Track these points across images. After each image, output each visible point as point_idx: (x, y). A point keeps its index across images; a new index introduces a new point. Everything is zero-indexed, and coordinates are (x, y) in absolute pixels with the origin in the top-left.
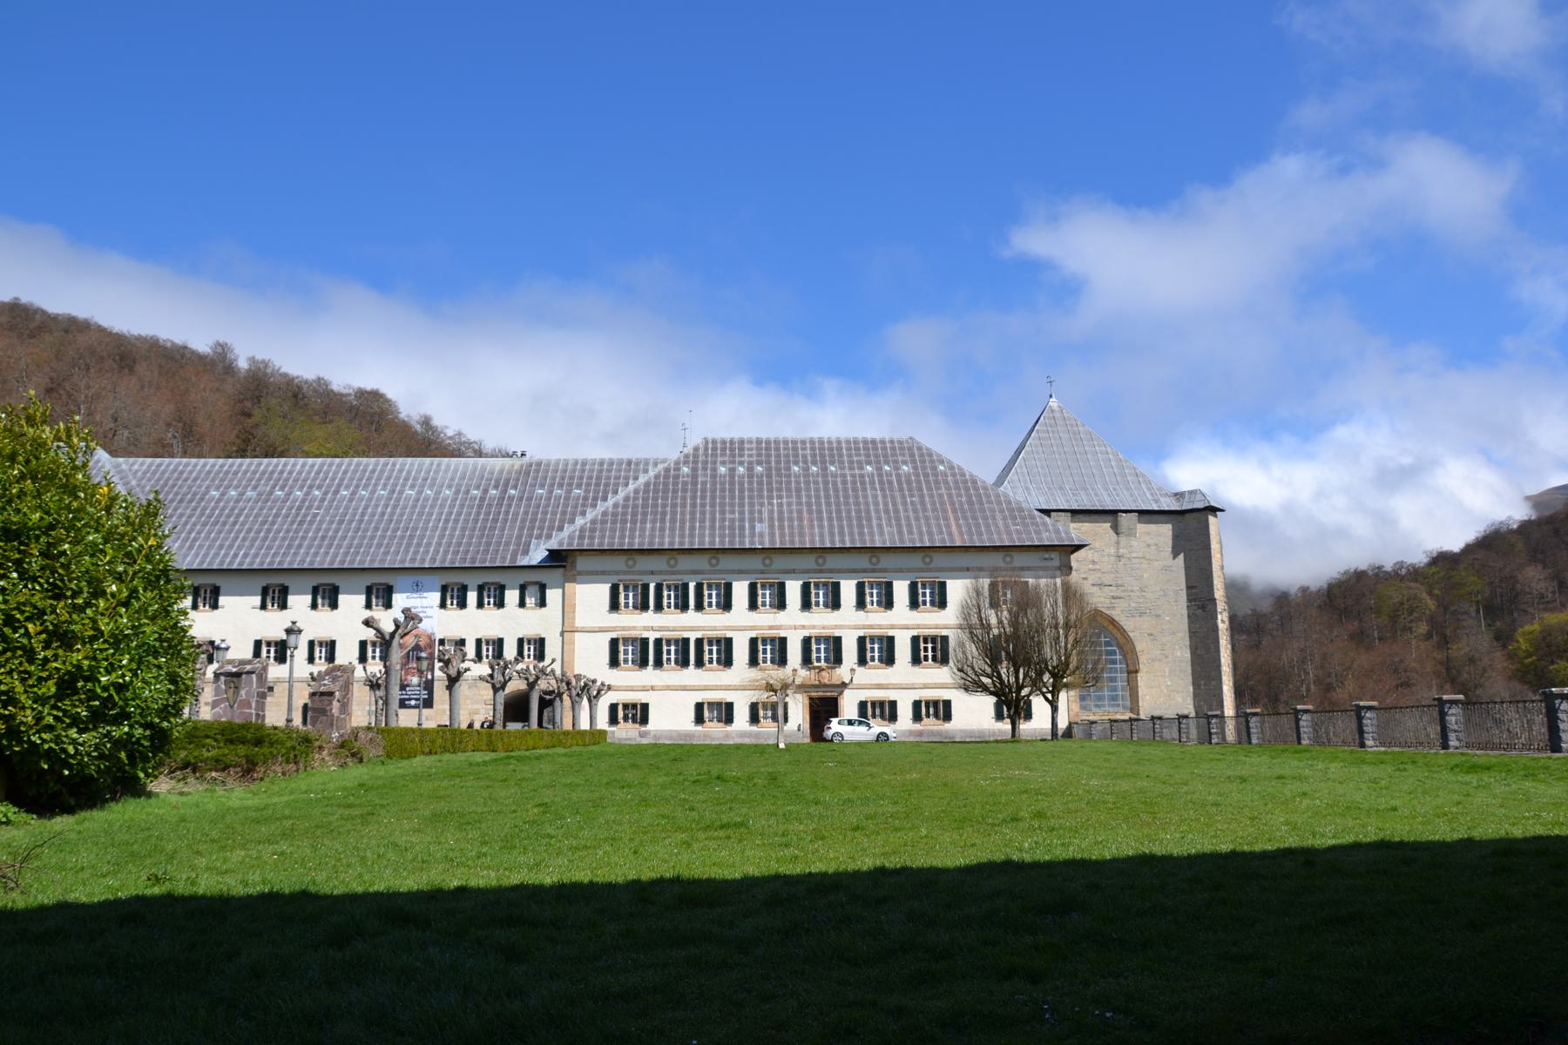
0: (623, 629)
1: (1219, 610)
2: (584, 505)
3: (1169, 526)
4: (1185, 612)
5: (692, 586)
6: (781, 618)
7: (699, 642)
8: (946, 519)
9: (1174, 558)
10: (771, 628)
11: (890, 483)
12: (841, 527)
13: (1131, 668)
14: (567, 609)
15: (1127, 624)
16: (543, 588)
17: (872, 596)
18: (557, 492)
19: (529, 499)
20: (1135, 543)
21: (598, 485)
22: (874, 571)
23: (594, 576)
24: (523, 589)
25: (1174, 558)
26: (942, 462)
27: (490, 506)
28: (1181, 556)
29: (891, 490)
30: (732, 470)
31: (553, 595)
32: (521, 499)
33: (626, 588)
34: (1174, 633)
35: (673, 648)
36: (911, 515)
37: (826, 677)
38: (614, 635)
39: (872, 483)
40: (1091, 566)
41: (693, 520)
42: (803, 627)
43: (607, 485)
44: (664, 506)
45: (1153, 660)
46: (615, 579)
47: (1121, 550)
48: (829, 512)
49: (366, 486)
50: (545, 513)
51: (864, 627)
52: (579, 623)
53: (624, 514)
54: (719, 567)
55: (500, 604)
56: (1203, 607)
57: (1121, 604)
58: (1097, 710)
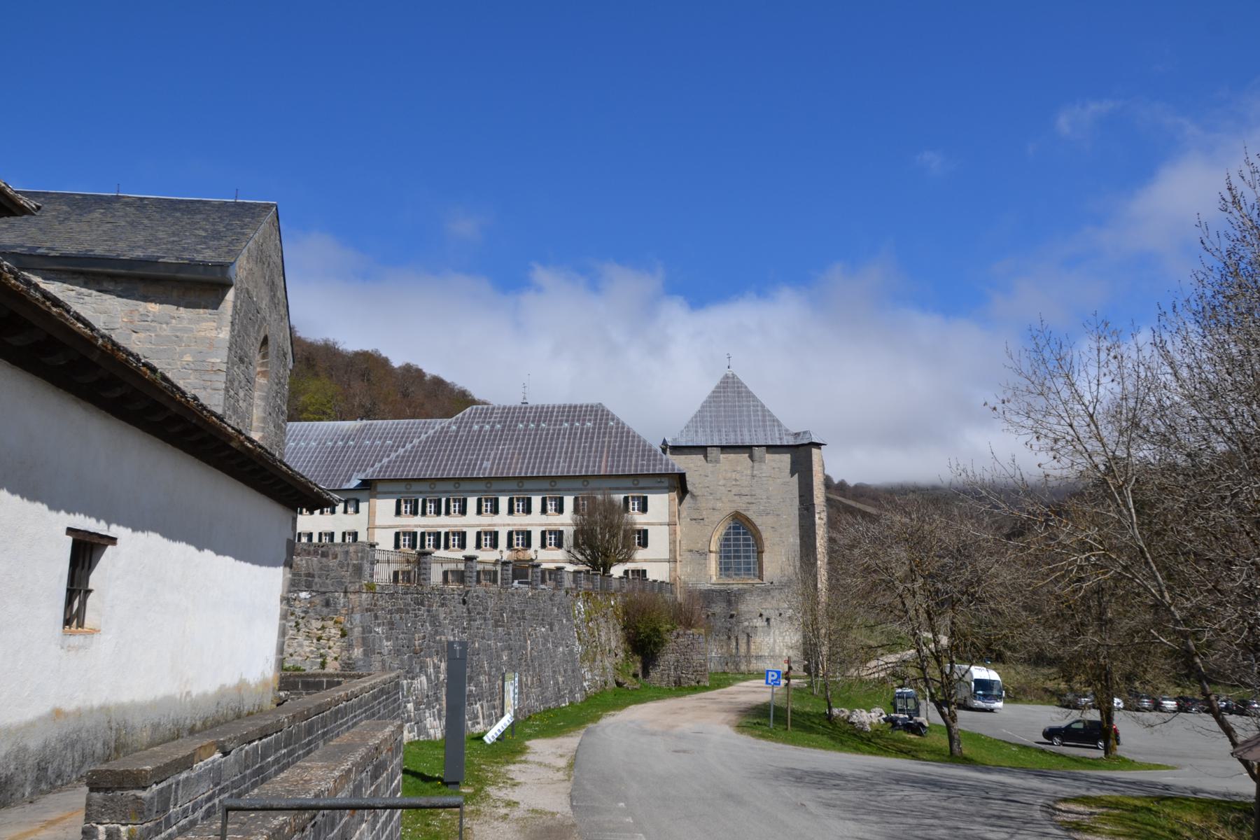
0: (403, 526)
1: (817, 511)
2: (390, 451)
3: (789, 456)
4: (797, 512)
5: (443, 500)
6: (496, 519)
7: (447, 534)
8: (601, 457)
9: (792, 476)
10: (489, 525)
11: (576, 434)
12: (535, 463)
13: (760, 550)
14: (371, 514)
15: (758, 521)
16: (357, 502)
17: (551, 507)
18: (377, 442)
19: (360, 447)
20: (765, 467)
21: (402, 438)
22: (552, 490)
23: (386, 495)
24: (346, 502)
25: (792, 476)
26: (613, 420)
27: (336, 452)
28: (797, 475)
29: (575, 439)
30: (482, 427)
31: (363, 506)
32: (354, 447)
33: (406, 502)
34: (788, 527)
35: (432, 538)
36: (581, 455)
37: (521, 556)
38: (397, 530)
39: (564, 434)
40: (734, 483)
41: (448, 460)
42: (509, 525)
43: (408, 437)
44: (434, 451)
45: (774, 545)
46: (399, 496)
47: (755, 472)
48: (531, 454)
49: (380, 438)
50: (366, 456)
51: (546, 525)
52: (378, 522)
53: (409, 457)
54: (460, 489)
55: (333, 512)
56: (807, 509)
57: (754, 507)
58: (736, 577)
